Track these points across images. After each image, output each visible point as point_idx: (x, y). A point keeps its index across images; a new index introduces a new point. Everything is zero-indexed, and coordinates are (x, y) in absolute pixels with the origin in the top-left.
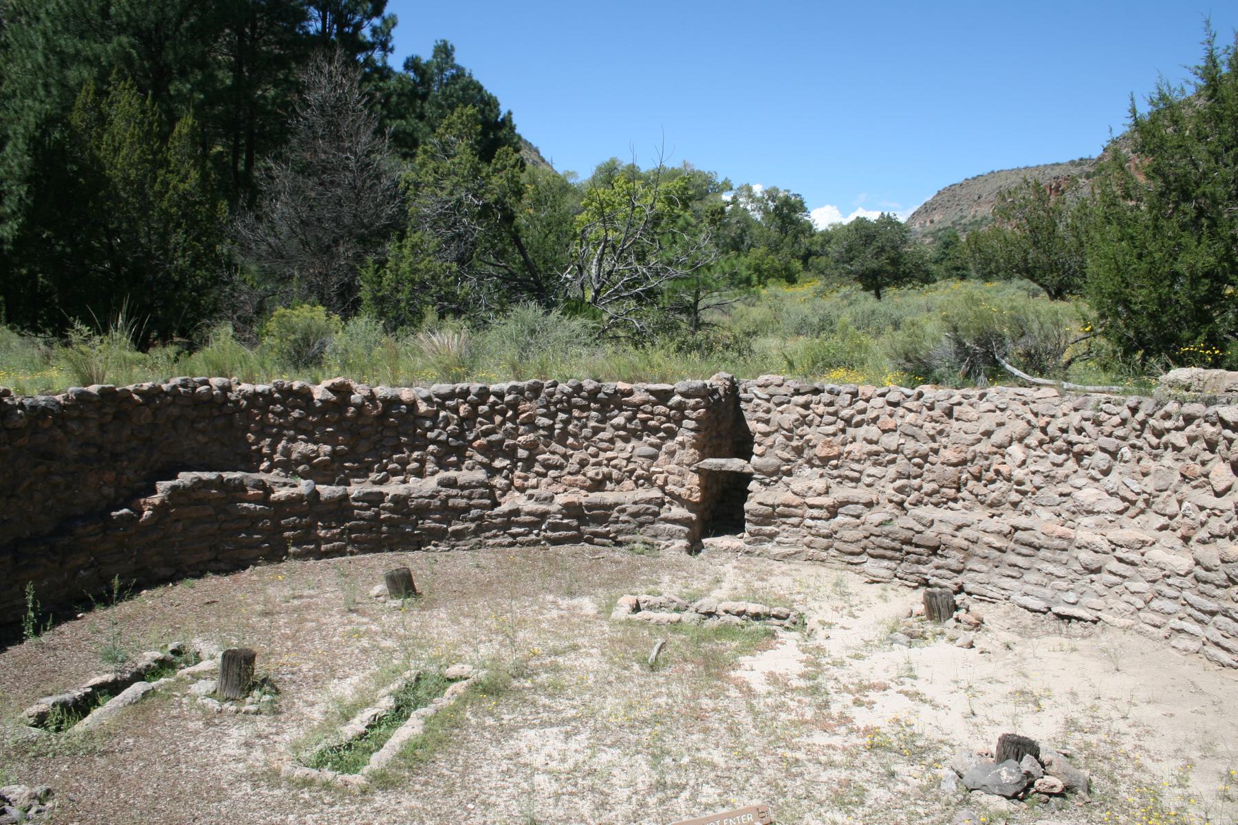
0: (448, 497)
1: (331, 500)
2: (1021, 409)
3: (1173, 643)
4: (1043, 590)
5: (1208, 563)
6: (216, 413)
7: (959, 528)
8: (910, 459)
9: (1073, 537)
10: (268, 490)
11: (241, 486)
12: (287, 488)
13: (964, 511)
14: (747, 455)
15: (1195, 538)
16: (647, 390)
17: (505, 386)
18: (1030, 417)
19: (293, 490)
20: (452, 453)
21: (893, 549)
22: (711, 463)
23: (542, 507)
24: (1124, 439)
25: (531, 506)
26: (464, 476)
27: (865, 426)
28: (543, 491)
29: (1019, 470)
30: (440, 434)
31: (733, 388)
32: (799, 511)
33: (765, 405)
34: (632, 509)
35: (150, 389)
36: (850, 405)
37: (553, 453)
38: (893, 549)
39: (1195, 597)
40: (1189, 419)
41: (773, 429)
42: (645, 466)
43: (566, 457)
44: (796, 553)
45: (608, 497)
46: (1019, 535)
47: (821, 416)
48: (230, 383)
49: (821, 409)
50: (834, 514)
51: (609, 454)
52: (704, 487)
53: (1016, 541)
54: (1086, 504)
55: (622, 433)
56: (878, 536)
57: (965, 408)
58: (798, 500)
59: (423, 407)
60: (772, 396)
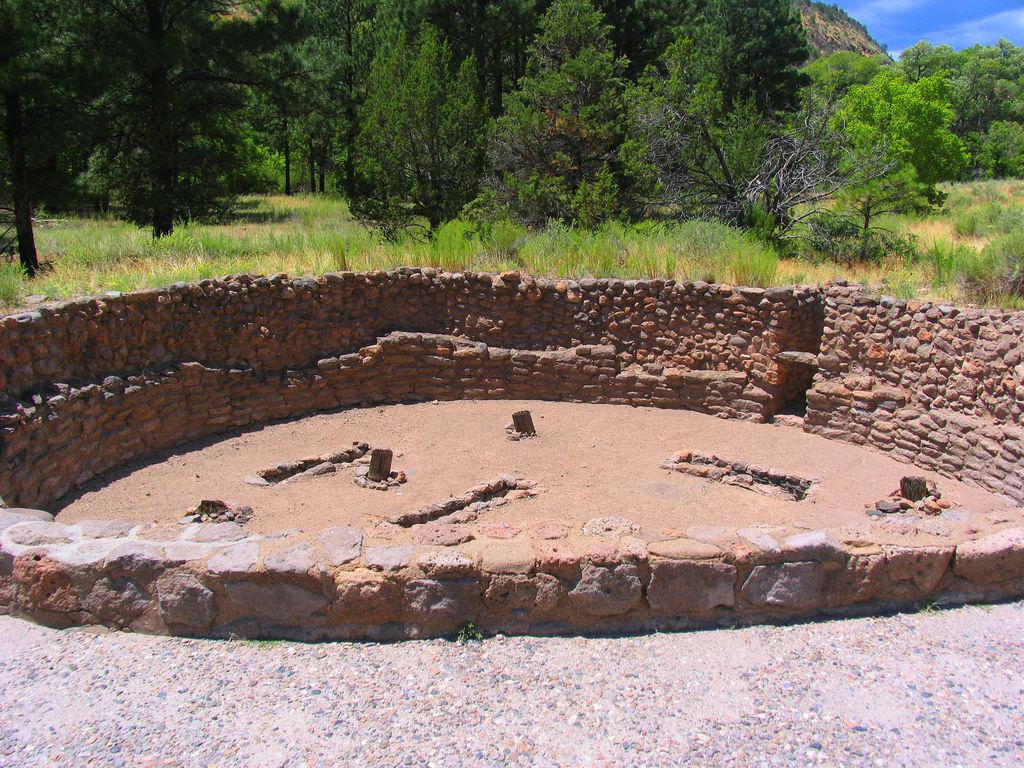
0: (584, 363)
1: (497, 358)
4: (1018, 491)
6: (424, 293)
7: (965, 430)
8: (938, 368)
10: (452, 347)
11: (434, 344)
13: (975, 416)
14: (816, 352)
16: (742, 293)
17: (635, 282)
20: (595, 330)
21: (913, 441)
25: (646, 376)
28: (656, 366)
30: (583, 316)
32: (848, 401)
34: (721, 385)
36: (897, 317)
37: (667, 337)
38: (913, 441)
41: (836, 331)
42: (736, 353)
43: (677, 340)
44: (842, 434)
45: (706, 374)
46: (1008, 443)
47: (874, 325)
50: (871, 409)
51: (711, 341)
53: (1004, 448)
56: (903, 429)
57: (990, 328)
58: (848, 392)
59: (571, 296)
60: (838, 304)
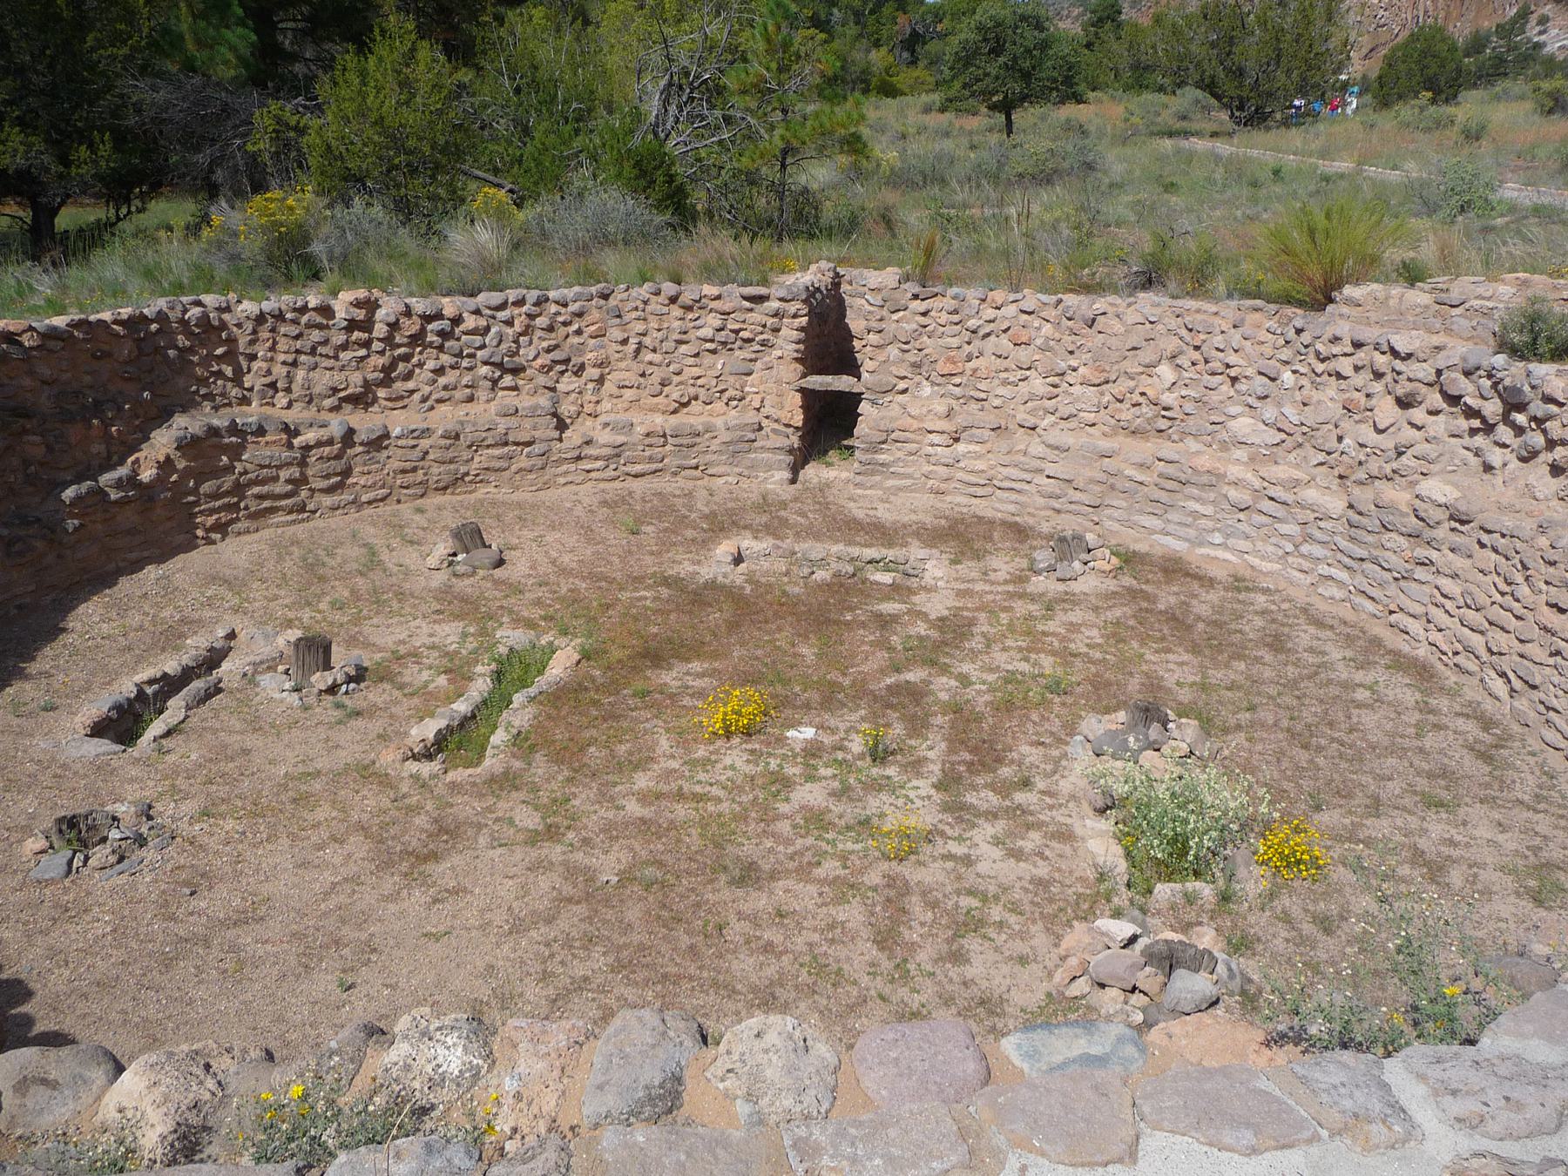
2: (1173, 323)
3: (1320, 590)
5: (1361, 508)
9: (1222, 471)
12: (315, 428)
15: (1353, 478)
18: (1184, 332)
22: (818, 382)
23: (621, 439)
26: (524, 402)
27: (992, 338)
33: (879, 313)
35: (131, 318)
39: (1346, 543)
40: (1358, 345)
48: (228, 302)
49: (944, 317)
52: (806, 407)
54: (1239, 434)
55: (709, 346)
58: (916, 425)
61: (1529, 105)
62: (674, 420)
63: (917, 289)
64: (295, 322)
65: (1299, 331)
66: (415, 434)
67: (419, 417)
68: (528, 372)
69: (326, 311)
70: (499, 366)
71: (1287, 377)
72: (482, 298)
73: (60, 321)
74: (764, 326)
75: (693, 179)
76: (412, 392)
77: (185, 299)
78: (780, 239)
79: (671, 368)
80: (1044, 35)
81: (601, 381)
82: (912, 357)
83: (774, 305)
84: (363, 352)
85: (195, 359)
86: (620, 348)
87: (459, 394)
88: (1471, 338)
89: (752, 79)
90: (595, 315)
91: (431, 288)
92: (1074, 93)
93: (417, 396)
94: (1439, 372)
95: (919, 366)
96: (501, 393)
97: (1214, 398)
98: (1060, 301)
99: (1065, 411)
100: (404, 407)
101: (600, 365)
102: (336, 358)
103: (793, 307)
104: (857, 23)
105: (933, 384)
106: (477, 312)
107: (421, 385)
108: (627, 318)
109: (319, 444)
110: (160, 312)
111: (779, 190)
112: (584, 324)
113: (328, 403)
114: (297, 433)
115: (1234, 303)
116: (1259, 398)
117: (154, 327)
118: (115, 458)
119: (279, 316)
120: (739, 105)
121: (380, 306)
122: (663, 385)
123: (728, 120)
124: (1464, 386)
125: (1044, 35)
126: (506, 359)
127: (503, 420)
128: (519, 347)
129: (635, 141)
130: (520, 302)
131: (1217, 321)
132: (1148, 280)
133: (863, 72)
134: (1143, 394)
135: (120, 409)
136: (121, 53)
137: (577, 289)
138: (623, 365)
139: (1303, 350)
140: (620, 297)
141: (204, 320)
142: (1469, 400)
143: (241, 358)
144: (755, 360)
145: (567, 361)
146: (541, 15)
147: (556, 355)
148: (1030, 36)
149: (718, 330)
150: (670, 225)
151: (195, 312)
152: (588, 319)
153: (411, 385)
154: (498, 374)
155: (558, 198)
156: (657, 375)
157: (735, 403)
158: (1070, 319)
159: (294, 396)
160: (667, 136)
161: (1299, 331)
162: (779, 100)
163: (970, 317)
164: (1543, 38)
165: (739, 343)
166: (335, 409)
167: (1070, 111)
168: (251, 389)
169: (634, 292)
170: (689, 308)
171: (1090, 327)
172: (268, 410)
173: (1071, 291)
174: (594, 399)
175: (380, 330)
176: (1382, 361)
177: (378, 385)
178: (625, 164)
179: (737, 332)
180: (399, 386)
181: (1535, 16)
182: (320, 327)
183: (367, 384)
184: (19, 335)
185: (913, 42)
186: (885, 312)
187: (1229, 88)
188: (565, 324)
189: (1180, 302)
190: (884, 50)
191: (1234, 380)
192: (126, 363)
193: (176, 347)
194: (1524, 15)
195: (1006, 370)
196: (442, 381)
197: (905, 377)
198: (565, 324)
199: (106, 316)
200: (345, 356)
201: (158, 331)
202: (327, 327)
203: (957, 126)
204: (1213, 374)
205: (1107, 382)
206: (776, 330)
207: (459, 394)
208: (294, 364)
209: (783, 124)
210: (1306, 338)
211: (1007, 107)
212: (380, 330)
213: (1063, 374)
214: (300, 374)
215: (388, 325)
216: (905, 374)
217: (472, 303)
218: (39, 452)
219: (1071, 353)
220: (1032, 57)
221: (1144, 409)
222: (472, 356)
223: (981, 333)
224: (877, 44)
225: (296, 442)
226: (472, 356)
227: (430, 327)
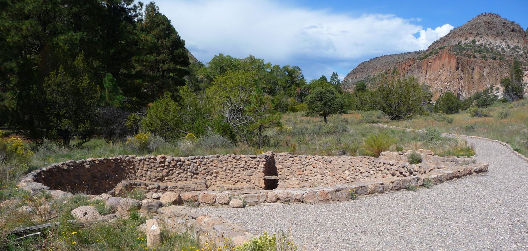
2: (348, 161)
18: (350, 163)
19: (153, 186)
22: (268, 177)
24: (371, 169)
26: (199, 181)
27: (308, 166)
29: (348, 177)
31: (273, 156)
35: (115, 159)
40: (384, 164)
49: (297, 162)
52: (265, 183)
55: (242, 169)
61: (469, 114)
62: (233, 186)
63: (291, 155)
64: (148, 161)
65: (373, 162)
66: (174, 187)
67: (174, 184)
68: (200, 174)
69: (155, 159)
70: (193, 173)
71: (372, 172)
72: (190, 157)
73: (102, 158)
74: (255, 164)
75: (237, 133)
76: (173, 178)
77: (125, 155)
78: (259, 148)
79: (233, 174)
80: (334, 96)
81: (216, 177)
82: (290, 171)
83: (258, 159)
84: (162, 169)
85: (127, 168)
86: (221, 169)
87: (183, 179)
88: (405, 161)
89: (252, 108)
90: (216, 161)
91: (177, 155)
92: (344, 111)
93: (174, 179)
94: (398, 168)
95: (292, 173)
96: (193, 179)
97: (357, 177)
98: (323, 158)
99: (325, 182)
100: (171, 182)
101: (217, 173)
102: (156, 170)
103: (262, 160)
104: (284, 90)
105: (295, 177)
106: (188, 160)
107: (175, 177)
108: (223, 162)
109: (152, 189)
110: (121, 158)
111: (259, 136)
112: (213, 163)
113: (154, 180)
114: (147, 186)
115: (360, 157)
116: (366, 177)
117: (119, 161)
118: (110, 189)
119: (145, 160)
120: (249, 115)
121: (167, 158)
122: (231, 178)
123: (246, 118)
124: (402, 170)
125: (334, 96)
126: (195, 171)
127: (194, 185)
128: (198, 168)
129: (223, 123)
130: (198, 158)
131: (357, 160)
132: (344, 153)
133: (286, 105)
134: (342, 178)
135: (112, 178)
136: (93, 101)
137: (212, 155)
138: (222, 173)
139: (374, 166)
140: (221, 157)
141: (129, 160)
142: (403, 173)
143: (136, 169)
144: (253, 172)
145: (209, 172)
146: (186, 88)
147: (206, 170)
148: (330, 96)
149: (244, 165)
150: (232, 143)
151: (127, 158)
152: (214, 162)
153: (173, 176)
154: (193, 174)
155: (204, 136)
156: (230, 176)
157: (248, 182)
158: (326, 161)
159: (146, 178)
160: (230, 122)
161: (373, 162)
162: (259, 113)
163: (303, 161)
164: (498, 94)
165: (249, 168)
166: (155, 181)
167: (344, 116)
168: (137, 176)
169: (225, 156)
170: (237, 160)
171: (330, 163)
172: (141, 181)
173: (326, 155)
174: (215, 181)
175: (167, 164)
176: (388, 166)
177: (165, 176)
178: (220, 129)
179: (249, 165)
180: (170, 177)
181: (495, 87)
182: (153, 162)
183: (163, 176)
184: (95, 161)
185: (302, 96)
186: (284, 161)
187: (387, 109)
188: (209, 163)
189: (349, 157)
190: (292, 98)
191: (361, 173)
192: (113, 168)
193: (123, 166)
194: (492, 87)
195: (312, 173)
196: (180, 176)
197: (289, 176)
198: (209, 163)
199: (111, 158)
200: (158, 169)
201: (120, 162)
202: (155, 163)
203: (312, 120)
204: (357, 172)
205: (334, 175)
206: (258, 165)
207: (183, 179)
208: (147, 171)
209: (260, 119)
210: (374, 163)
211: (325, 115)
212: (167, 164)
213: (325, 174)
214: (148, 173)
215: (169, 162)
216: (289, 175)
217: (187, 158)
218: (97, 185)
219: (326, 169)
220: (331, 102)
221: (343, 181)
222: (187, 170)
223: (306, 165)
224: (290, 96)
225: (147, 188)
226: (187, 170)
227: (178, 163)
